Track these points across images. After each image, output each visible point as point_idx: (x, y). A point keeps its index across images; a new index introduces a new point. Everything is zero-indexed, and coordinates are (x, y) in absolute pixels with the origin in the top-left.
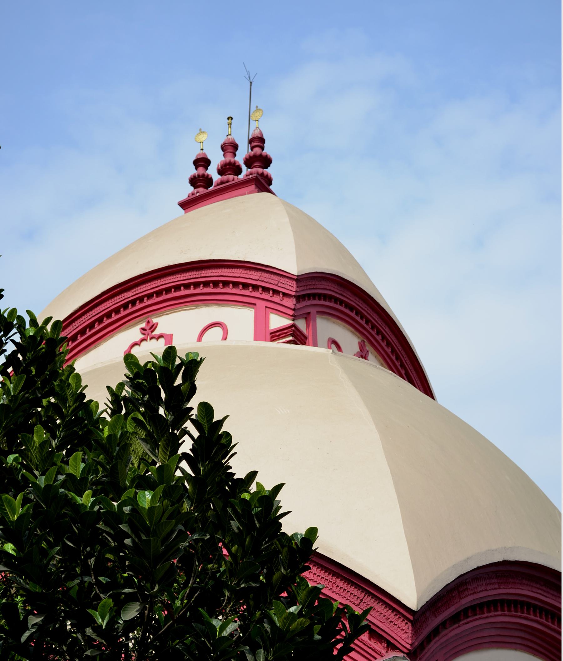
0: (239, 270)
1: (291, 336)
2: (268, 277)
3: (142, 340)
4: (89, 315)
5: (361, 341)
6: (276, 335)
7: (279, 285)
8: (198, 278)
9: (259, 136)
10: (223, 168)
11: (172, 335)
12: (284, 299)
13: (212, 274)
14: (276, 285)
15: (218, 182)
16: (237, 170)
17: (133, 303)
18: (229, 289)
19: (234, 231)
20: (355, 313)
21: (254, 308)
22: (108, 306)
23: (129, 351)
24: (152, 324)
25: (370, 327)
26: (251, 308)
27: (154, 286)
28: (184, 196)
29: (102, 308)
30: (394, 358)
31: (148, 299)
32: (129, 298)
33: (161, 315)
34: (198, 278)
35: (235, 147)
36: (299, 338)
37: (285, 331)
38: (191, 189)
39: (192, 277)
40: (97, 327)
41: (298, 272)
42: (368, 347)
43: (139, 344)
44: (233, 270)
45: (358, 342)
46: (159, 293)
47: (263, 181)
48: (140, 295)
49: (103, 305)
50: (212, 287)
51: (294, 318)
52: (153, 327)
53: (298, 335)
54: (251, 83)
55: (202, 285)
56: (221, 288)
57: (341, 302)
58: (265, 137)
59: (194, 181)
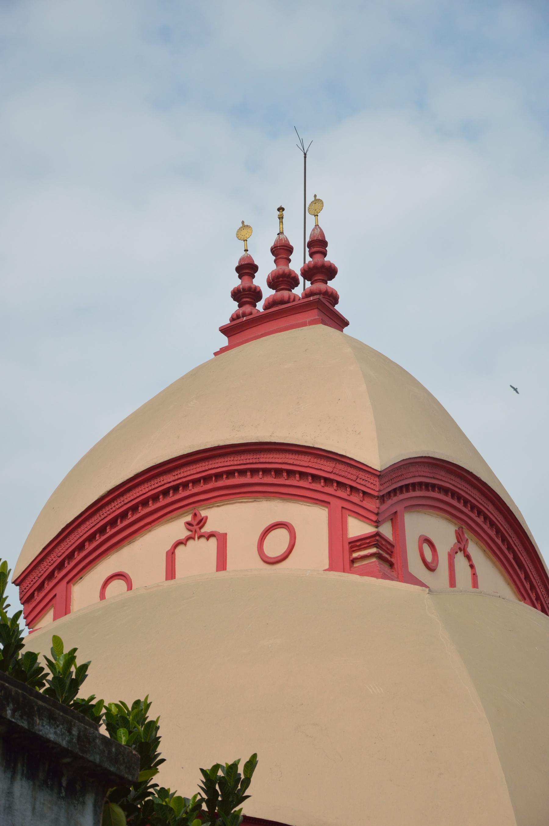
0: (306, 457)
1: (375, 547)
2: (343, 470)
3: (188, 538)
4: (120, 502)
5: (459, 528)
7: (358, 481)
8: (256, 463)
9: (320, 238)
10: (276, 281)
11: (226, 534)
12: (365, 499)
13: (273, 460)
14: (354, 481)
15: (270, 302)
17: (176, 489)
18: (295, 481)
19: (298, 403)
20: (450, 497)
21: (327, 507)
22: (144, 491)
23: (172, 551)
24: (200, 518)
25: (470, 509)
26: (324, 506)
27: (201, 469)
28: (226, 321)
29: (136, 493)
30: (499, 542)
31: (193, 486)
32: (170, 482)
33: (211, 506)
34: (256, 463)
35: (289, 249)
36: (384, 548)
37: (368, 541)
38: (233, 307)
39: (248, 461)
41: (381, 469)
42: (468, 535)
43: (185, 543)
44: (300, 456)
45: (455, 530)
46: (207, 479)
48: (184, 480)
49: (137, 490)
50: (274, 477)
51: (377, 524)
52: (202, 522)
53: (382, 544)
54: (305, 154)
55: (261, 473)
56: (286, 478)
58: (327, 239)
59: (237, 295)
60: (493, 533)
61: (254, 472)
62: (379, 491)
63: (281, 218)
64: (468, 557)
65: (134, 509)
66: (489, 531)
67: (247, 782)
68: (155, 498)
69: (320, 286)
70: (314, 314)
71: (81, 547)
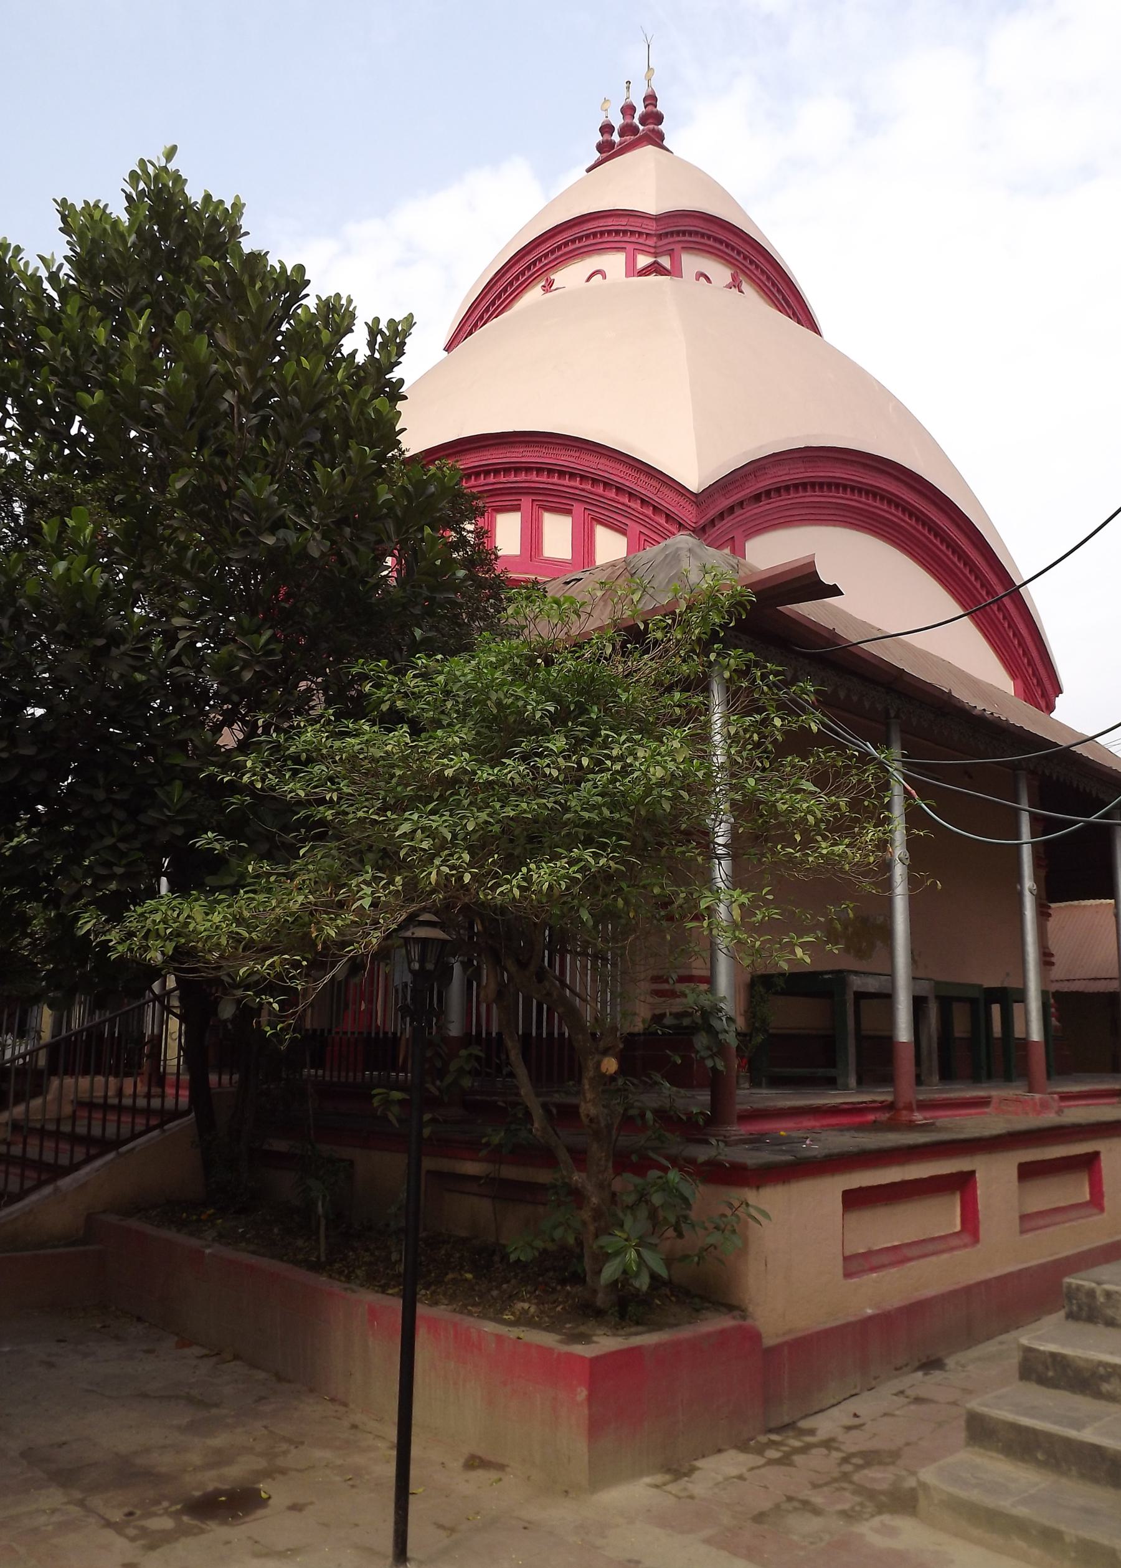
6: (645, 272)
18: (606, 238)
30: (769, 285)
42: (741, 277)
46: (553, 252)
47: (653, 136)
52: (551, 283)
60: (764, 278)
61: (580, 239)
62: (656, 230)
63: (628, 88)
66: (761, 277)
67: (406, 334)
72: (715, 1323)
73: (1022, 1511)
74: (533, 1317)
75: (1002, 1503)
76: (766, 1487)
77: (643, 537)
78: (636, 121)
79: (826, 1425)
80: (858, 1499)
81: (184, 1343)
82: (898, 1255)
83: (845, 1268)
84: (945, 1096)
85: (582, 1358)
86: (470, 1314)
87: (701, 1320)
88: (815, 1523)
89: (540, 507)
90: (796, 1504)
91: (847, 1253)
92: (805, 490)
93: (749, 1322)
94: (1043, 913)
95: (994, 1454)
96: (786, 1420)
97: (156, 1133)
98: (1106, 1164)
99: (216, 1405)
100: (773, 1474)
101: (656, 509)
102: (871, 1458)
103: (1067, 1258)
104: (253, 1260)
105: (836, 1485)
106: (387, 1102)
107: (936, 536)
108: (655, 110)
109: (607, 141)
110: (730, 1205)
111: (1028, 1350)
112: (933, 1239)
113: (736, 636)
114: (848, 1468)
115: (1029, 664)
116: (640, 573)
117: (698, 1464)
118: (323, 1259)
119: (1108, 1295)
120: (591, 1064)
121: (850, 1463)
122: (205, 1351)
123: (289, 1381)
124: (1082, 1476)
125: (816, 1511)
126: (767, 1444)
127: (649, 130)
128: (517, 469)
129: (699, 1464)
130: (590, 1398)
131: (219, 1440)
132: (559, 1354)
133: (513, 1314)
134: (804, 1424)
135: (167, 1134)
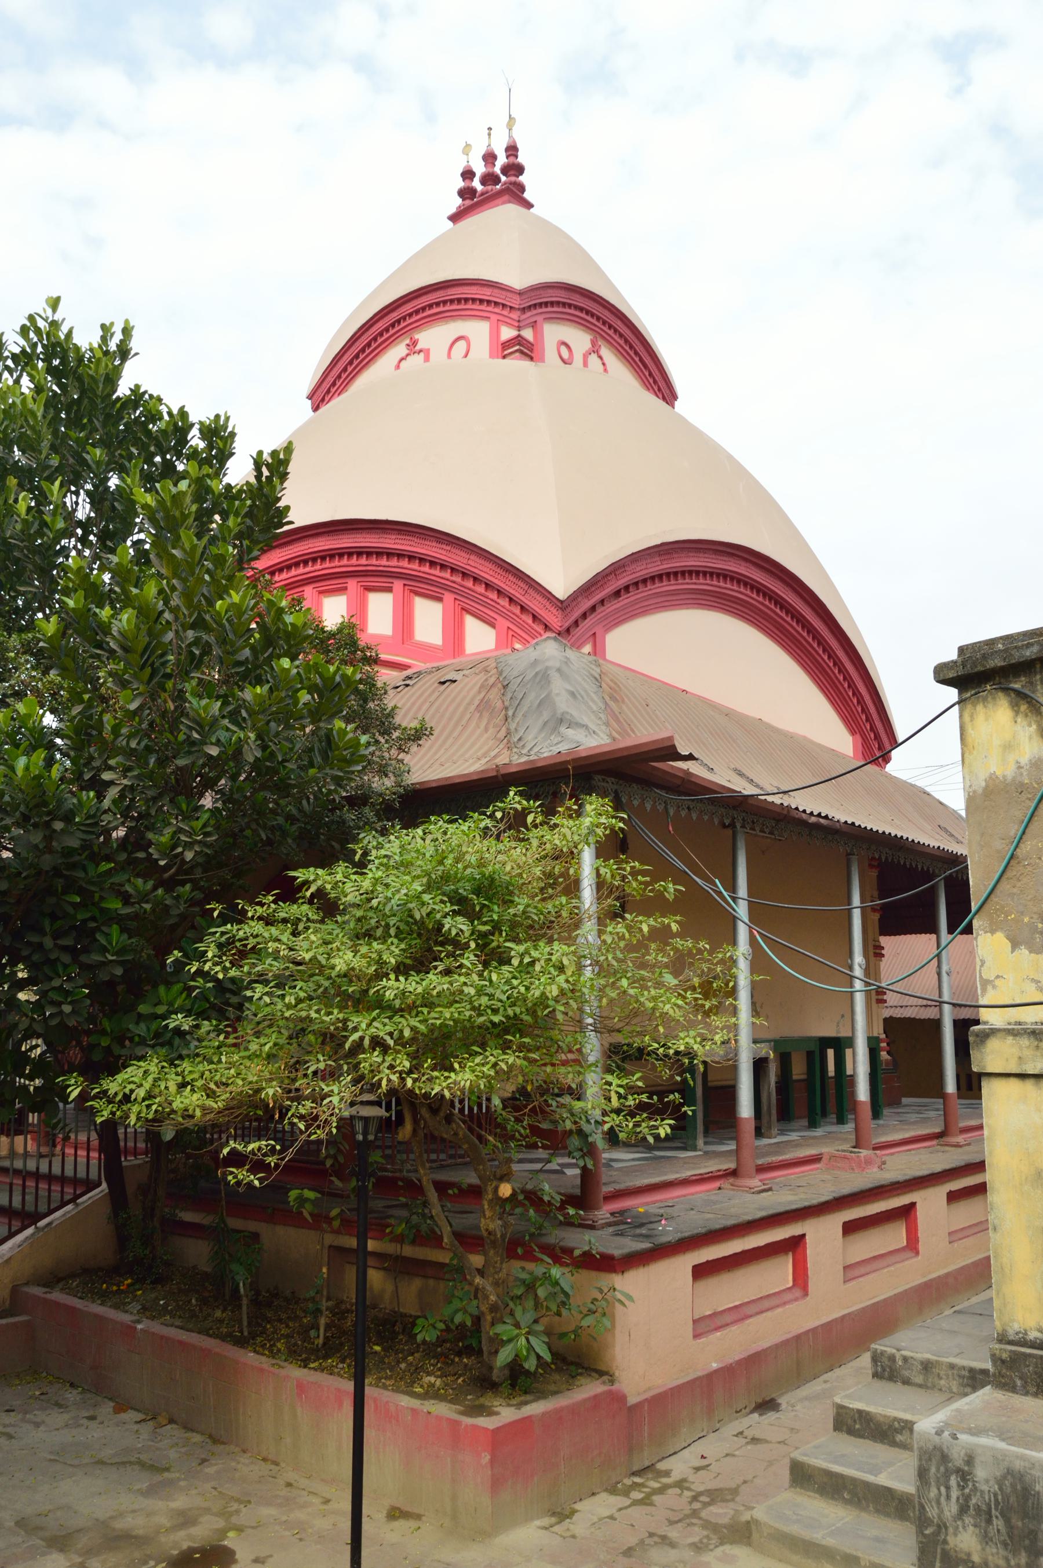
3: (408, 355)
16: (496, 180)
17: (399, 321)
18: (469, 306)
28: (453, 210)
30: (627, 348)
40: (374, 346)
42: (600, 342)
46: (417, 312)
51: (519, 328)
52: (415, 343)
57: (570, 306)
58: (519, 146)
60: (622, 342)
61: (445, 302)
63: (489, 135)
64: (601, 357)
65: (375, 339)
66: (619, 340)
68: (387, 330)
69: (513, 179)
70: (506, 197)
71: (345, 370)
72: (589, 1389)
73: (830, 1542)
74: (439, 1389)
75: (815, 1536)
76: (633, 1526)
77: (511, 633)
78: (497, 169)
79: (678, 1466)
80: (705, 1533)
81: (119, 1409)
82: (739, 1313)
83: (694, 1330)
84: (781, 1158)
85: (486, 1429)
86: (385, 1387)
87: (578, 1386)
88: (673, 1554)
89: (411, 591)
90: (656, 1539)
91: (696, 1317)
92: (661, 580)
93: (615, 1387)
94: (874, 952)
95: (812, 1494)
96: (647, 1463)
97: (70, 1207)
98: (921, 1212)
99: (167, 1470)
100: (637, 1512)
101: (523, 609)
102: (715, 1496)
103: (885, 1300)
104: (183, 1336)
105: (688, 1521)
106: (302, 1200)
107: (781, 609)
108: (516, 161)
109: (468, 188)
110: (601, 1291)
111: (840, 1407)
112: (768, 1296)
113: (604, 780)
114: (697, 1505)
115: (867, 720)
116: (513, 687)
117: (577, 1506)
118: (246, 1334)
119: (905, 1359)
120: (490, 1189)
121: (698, 1501)
122: (141, 1416)
123: (224, 1443)
124: (877, 1511)
125: (673, 1545)
126: (631, 1486)
127: (511, 183)
128: (389, 554)
129: (578, 1506)
130: (492, 1461)
131: (180, 1502)
132: (467, 1426)
133: (422, 1386)
134: (662, 1466)
135: (81, 1208)
